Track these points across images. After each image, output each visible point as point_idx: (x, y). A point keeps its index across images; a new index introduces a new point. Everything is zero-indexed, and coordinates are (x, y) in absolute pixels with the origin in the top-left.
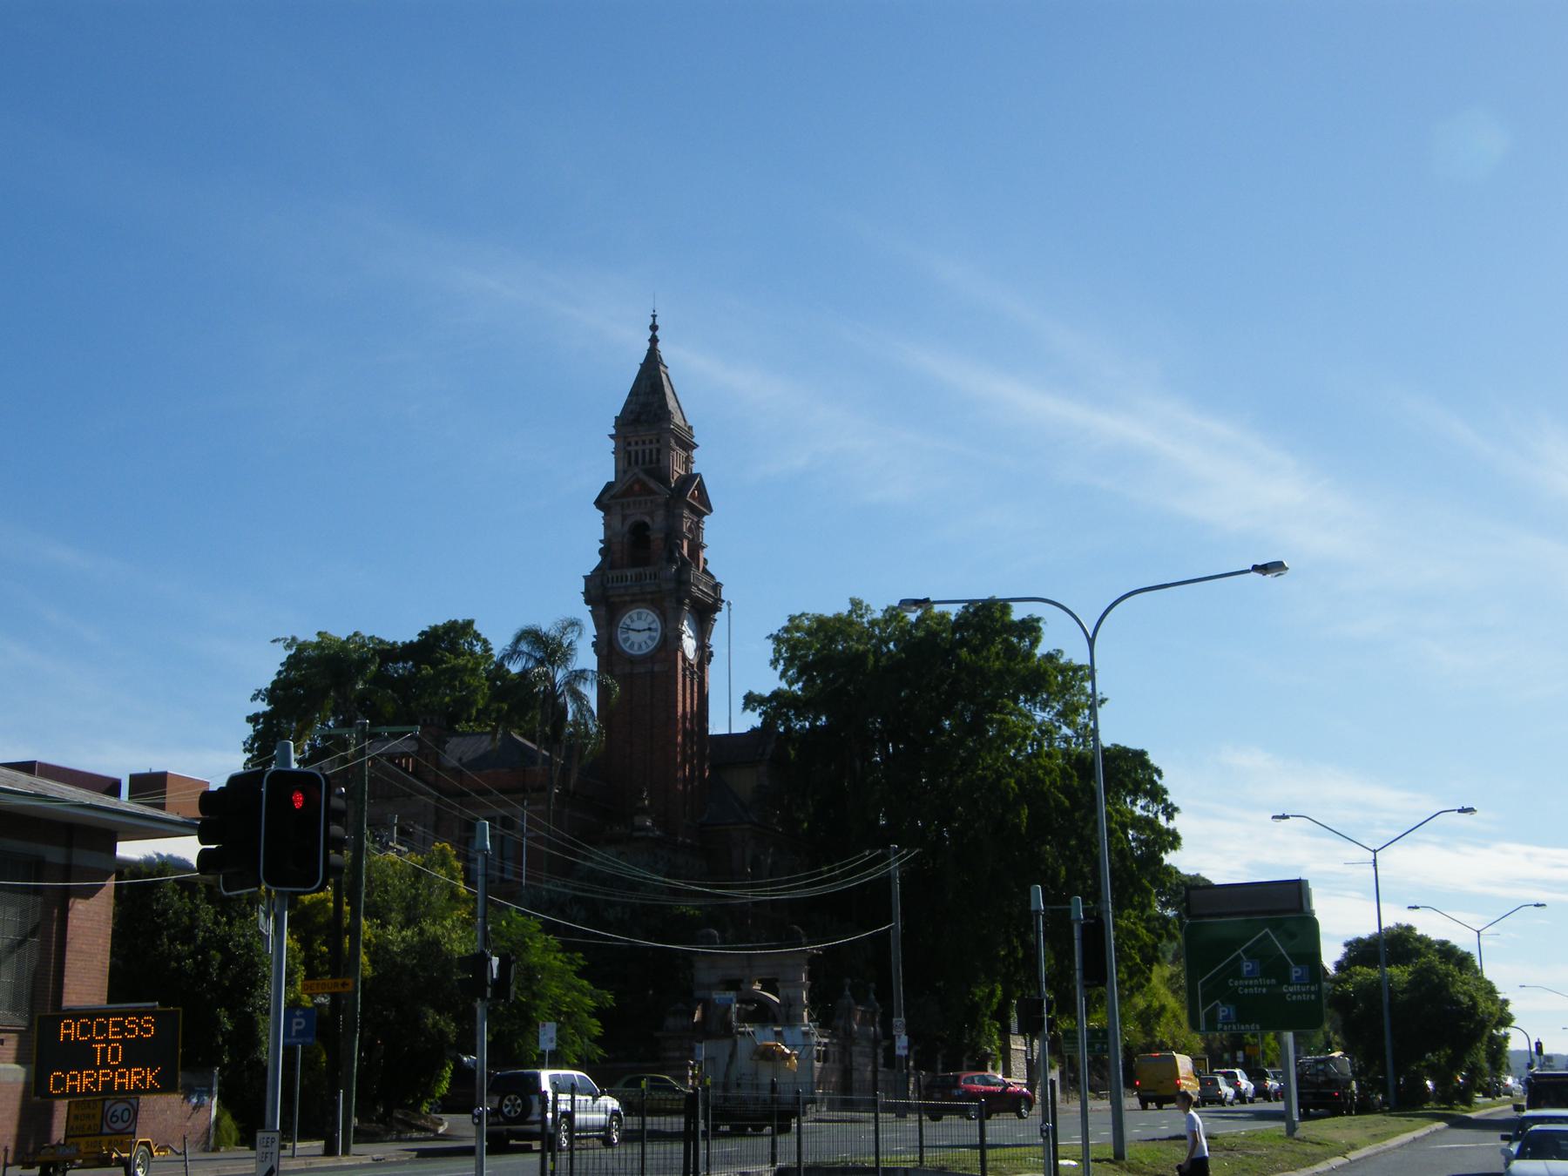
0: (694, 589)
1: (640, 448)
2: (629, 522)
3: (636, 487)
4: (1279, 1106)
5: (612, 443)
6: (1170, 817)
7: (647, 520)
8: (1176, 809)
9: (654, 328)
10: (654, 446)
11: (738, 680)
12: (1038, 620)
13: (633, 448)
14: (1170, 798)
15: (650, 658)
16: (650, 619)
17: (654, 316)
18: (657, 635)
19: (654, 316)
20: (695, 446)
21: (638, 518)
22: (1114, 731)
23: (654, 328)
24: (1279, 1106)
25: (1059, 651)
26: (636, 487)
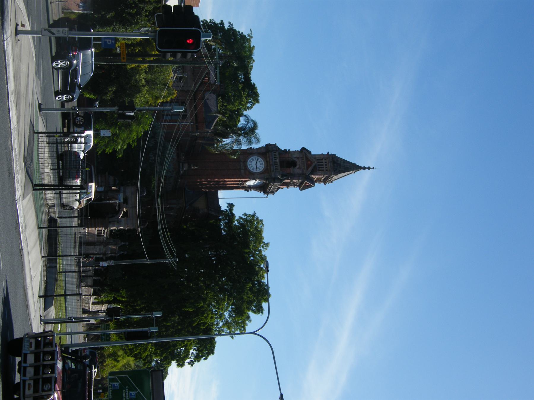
0: (272, 184)
1: (324, 164)
2: (296, 160)
3: (309, 162)
5: (326, 153)
6: (189, 363)
7: (297, 167)
8: (192, 365)
9: (369, 168)
10: (325, 169)
11: (238, 201)
14: (196, 363)
16: (260, 168)
17: (373, 168)
19: (373, 168)
23: (369, 168)
26: (309, 162)
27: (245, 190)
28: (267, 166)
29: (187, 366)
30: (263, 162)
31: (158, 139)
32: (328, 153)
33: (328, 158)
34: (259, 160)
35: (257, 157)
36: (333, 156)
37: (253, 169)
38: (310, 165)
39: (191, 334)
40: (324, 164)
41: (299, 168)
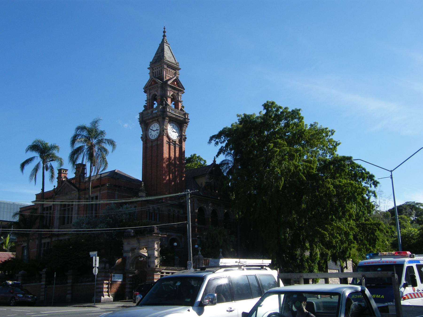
0: (168, 113)
1: (157, 70)
2: (151, 95)
3: (153, 83)
4: (97, 290)
5: (149, 71)
6: (376, 186)
7: (156, 93)
8: (378, 183)
9: (164, 32)
10: (160, 69)
11: (203, 147)
12: (299, 110)
13: (153, 71)
14: (375, 179)
15: (157, 139)
16: (157, 126)
17: (164, 28)
18: (158, 131)
19: (164, 28)
20: (179, 69)
21: (154, 93)
22: (340, 152)
23: (164, 32)
24: (97, 290)
25: (315, 123)
26: (153, 83)
27: (185, 141)
28: (175, 122)
29: (284, 107)
30: (153, 125)
31: (303, 178)
32: (148, 68)
33: (152, 68)
34: (151, 128)
35: (150, 131)
36: (152, 64)
37: (157, 133)
38: (155, 81)
39: (344, 182)
40: (157, 70)
41: (157, 91)
